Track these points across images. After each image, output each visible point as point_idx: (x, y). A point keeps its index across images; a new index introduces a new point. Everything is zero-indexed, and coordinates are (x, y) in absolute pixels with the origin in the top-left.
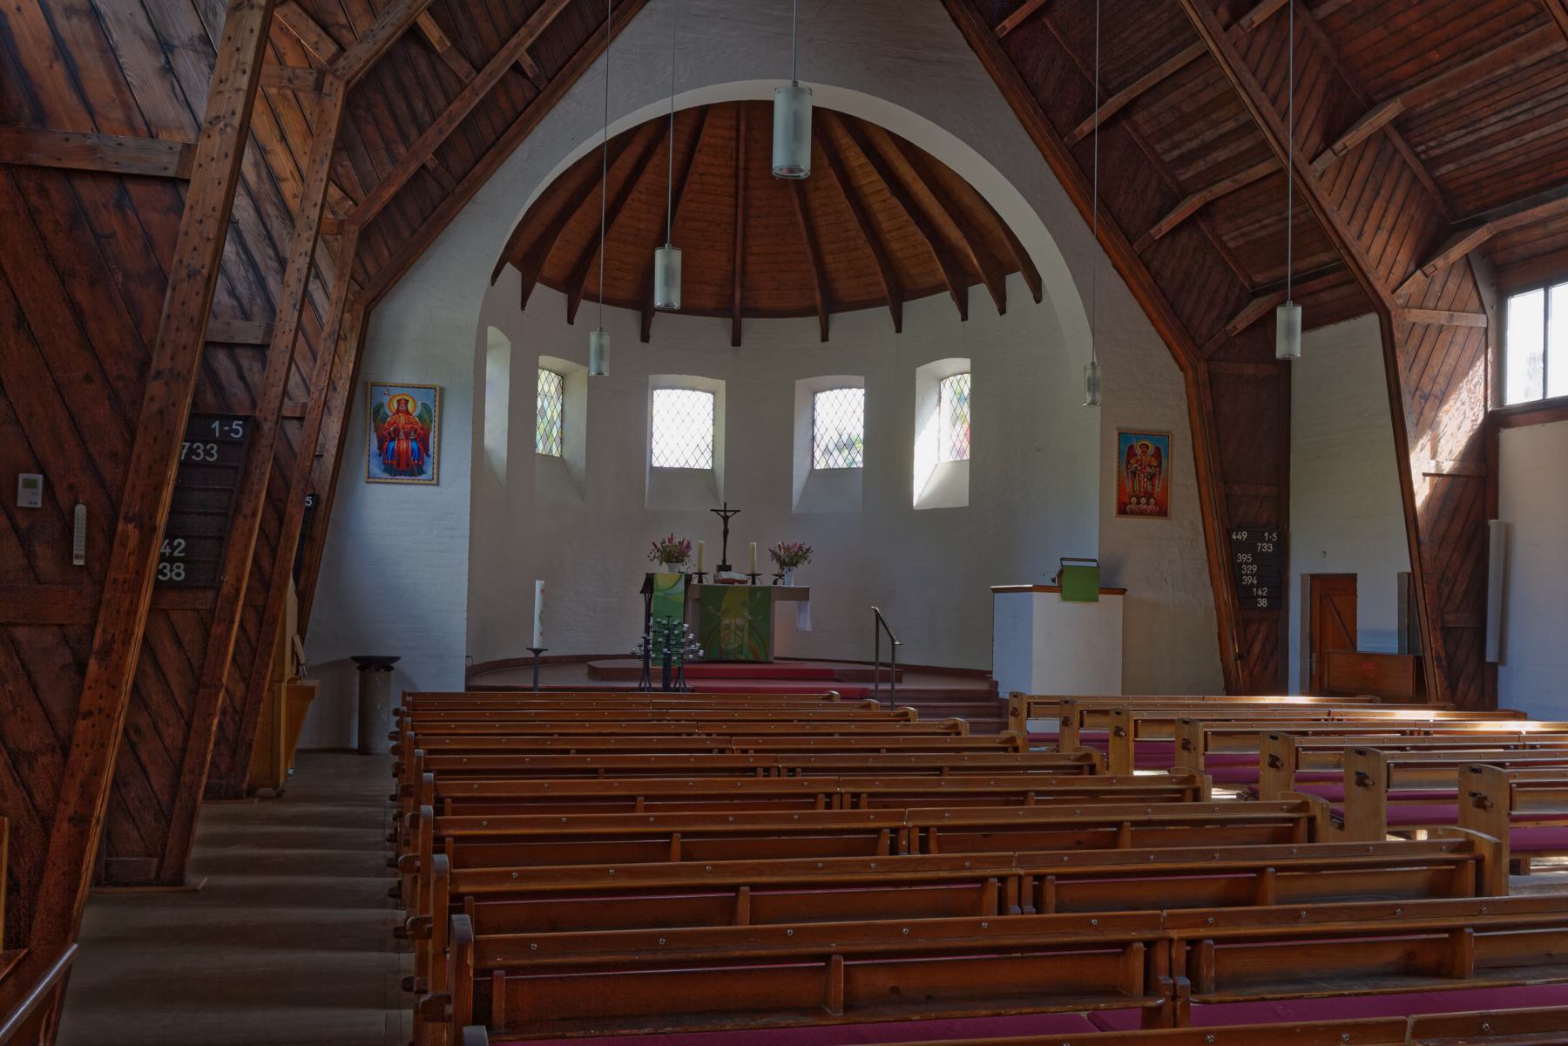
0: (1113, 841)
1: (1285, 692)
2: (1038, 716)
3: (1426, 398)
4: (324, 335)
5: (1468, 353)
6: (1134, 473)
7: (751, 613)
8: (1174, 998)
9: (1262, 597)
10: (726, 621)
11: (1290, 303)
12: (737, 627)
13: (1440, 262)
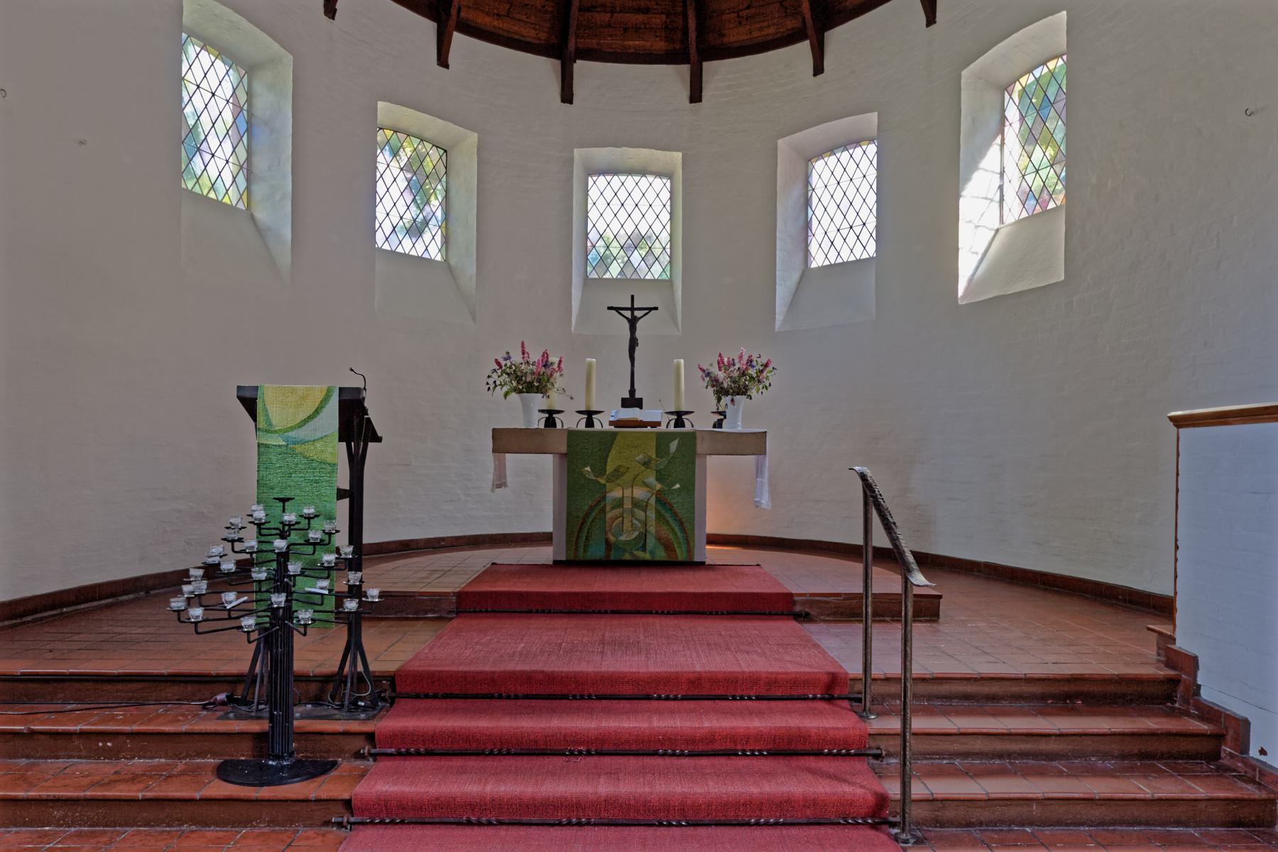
7: (659, 479)
10: (616, 493)
12: (636, 504)
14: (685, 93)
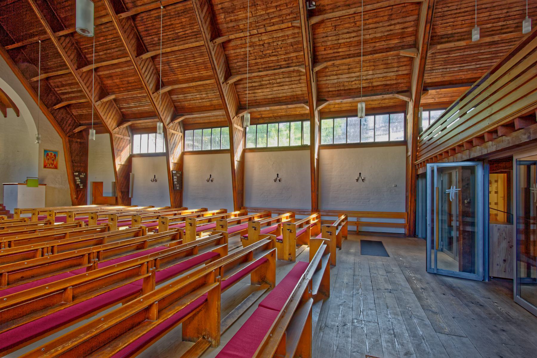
0: (64, 237)
1: (86, 204)
2: (23, 213)
3: (119, 150)
5: (127, 143)
6: (48, 159)
8: (95, 263)
11: (93, 129)
13: (122, 127)
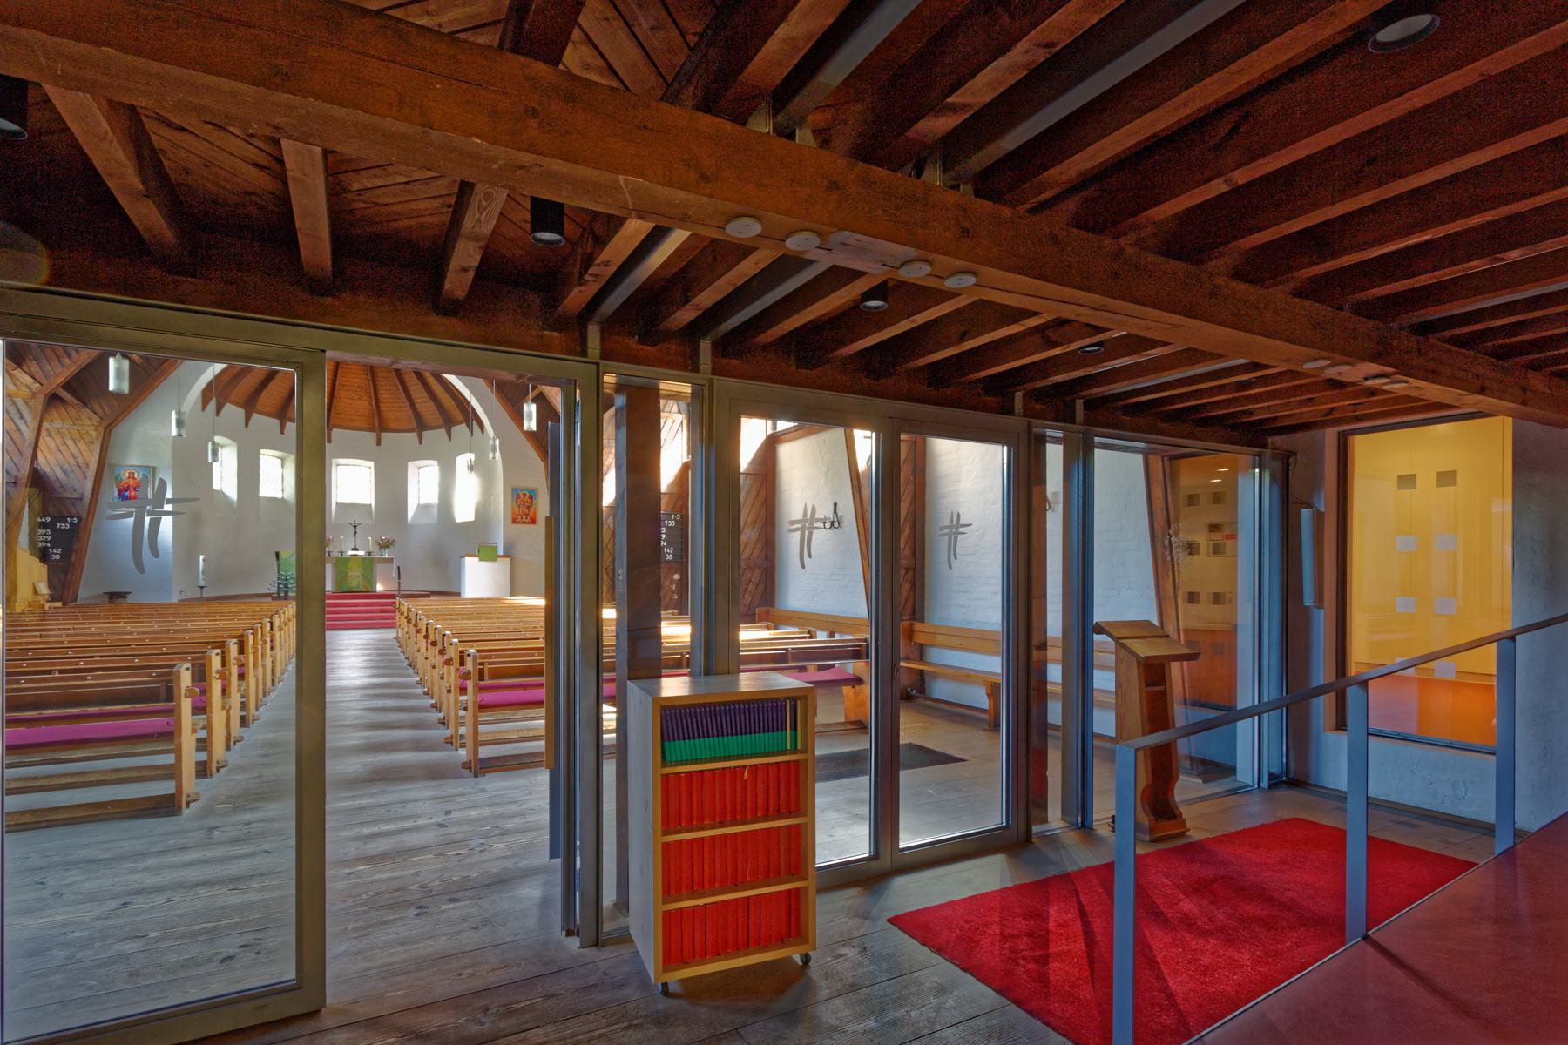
4: (26, 444)
9: (669, 554)
10: (350, 574)
14: (374, 442)
